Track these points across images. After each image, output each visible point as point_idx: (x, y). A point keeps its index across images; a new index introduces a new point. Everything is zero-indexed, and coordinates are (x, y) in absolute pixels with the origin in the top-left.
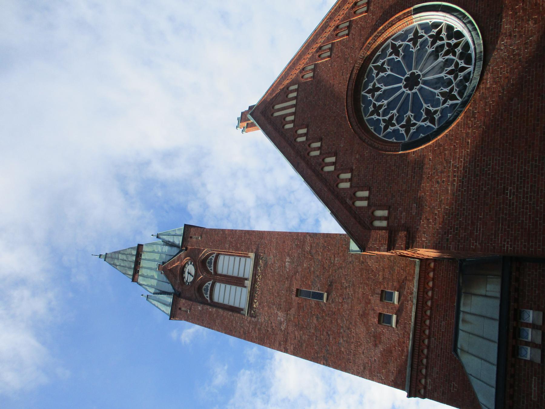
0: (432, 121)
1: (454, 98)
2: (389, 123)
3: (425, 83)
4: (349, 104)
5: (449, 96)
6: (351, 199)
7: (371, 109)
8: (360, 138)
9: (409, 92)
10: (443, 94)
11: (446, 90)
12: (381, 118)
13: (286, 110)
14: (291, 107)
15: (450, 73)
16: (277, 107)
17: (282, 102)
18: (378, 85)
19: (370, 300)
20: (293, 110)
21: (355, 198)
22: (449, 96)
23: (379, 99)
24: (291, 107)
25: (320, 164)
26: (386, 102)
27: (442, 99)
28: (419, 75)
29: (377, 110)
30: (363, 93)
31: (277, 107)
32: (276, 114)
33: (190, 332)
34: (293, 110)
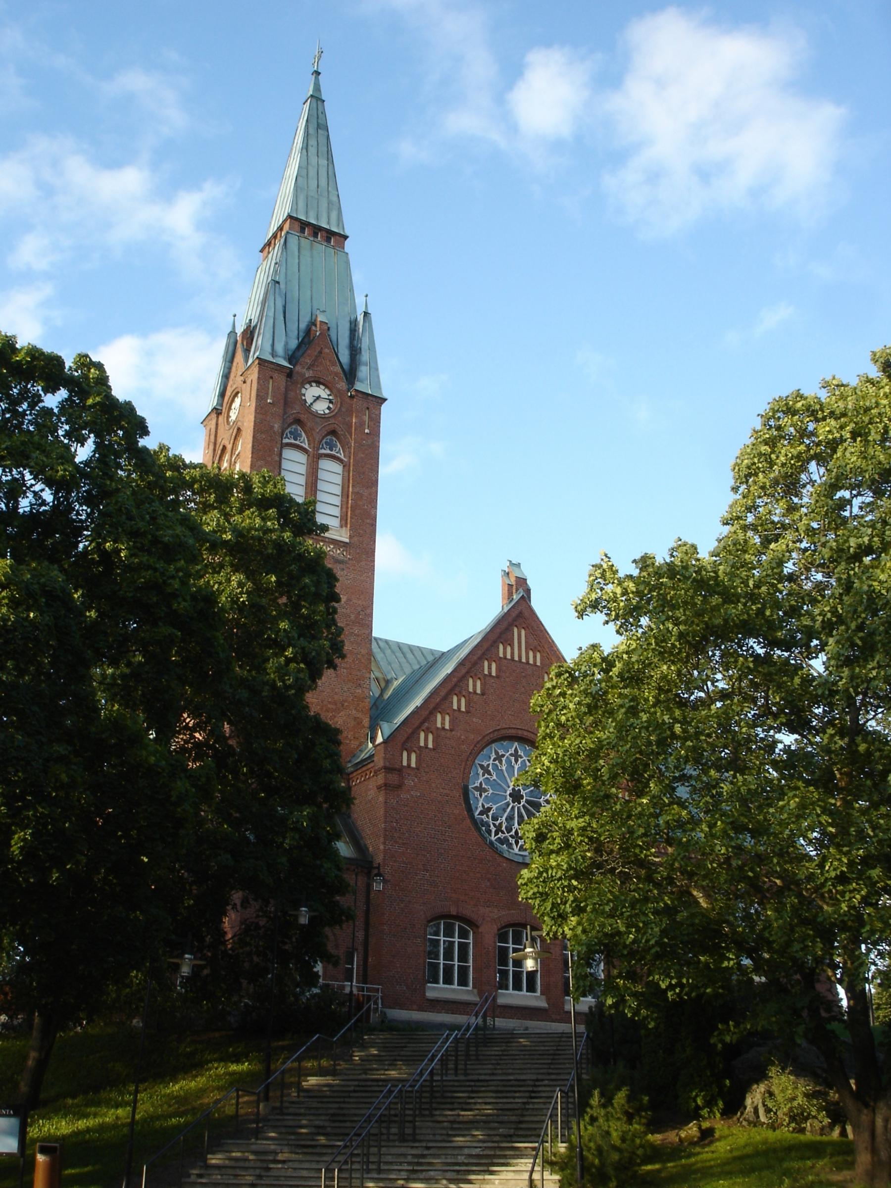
0: (481, 813)
1: (496, 833)
2: (486, 771)
3: (513, 808)
4: (510, 731)
5: (499, 829)
6: (428, 729)
7: (501, 752)
8: (478, 742)
9: (508, 792)
10: (501, 824)
11: (503, 828)
12: (491, 762)
13: (517, 649)
14: (520, 656)
15: (516, 761)
16: (523, 632)
17: (526, 642)
18: (520, 760)
19: (219, 573)
20: (516, 658)
21: (427, 731)
22: (499, 829)
23: (509, 830)
24: (520, 656)
25: (460, 692)
26: (504, 768)
27: (497, 823)
28: (519, 803)
29: (499, 758)
30: (516, 743)
31: (523, 632)
32: (516, 630)
33: (220, 346)
34: (516, 658)
